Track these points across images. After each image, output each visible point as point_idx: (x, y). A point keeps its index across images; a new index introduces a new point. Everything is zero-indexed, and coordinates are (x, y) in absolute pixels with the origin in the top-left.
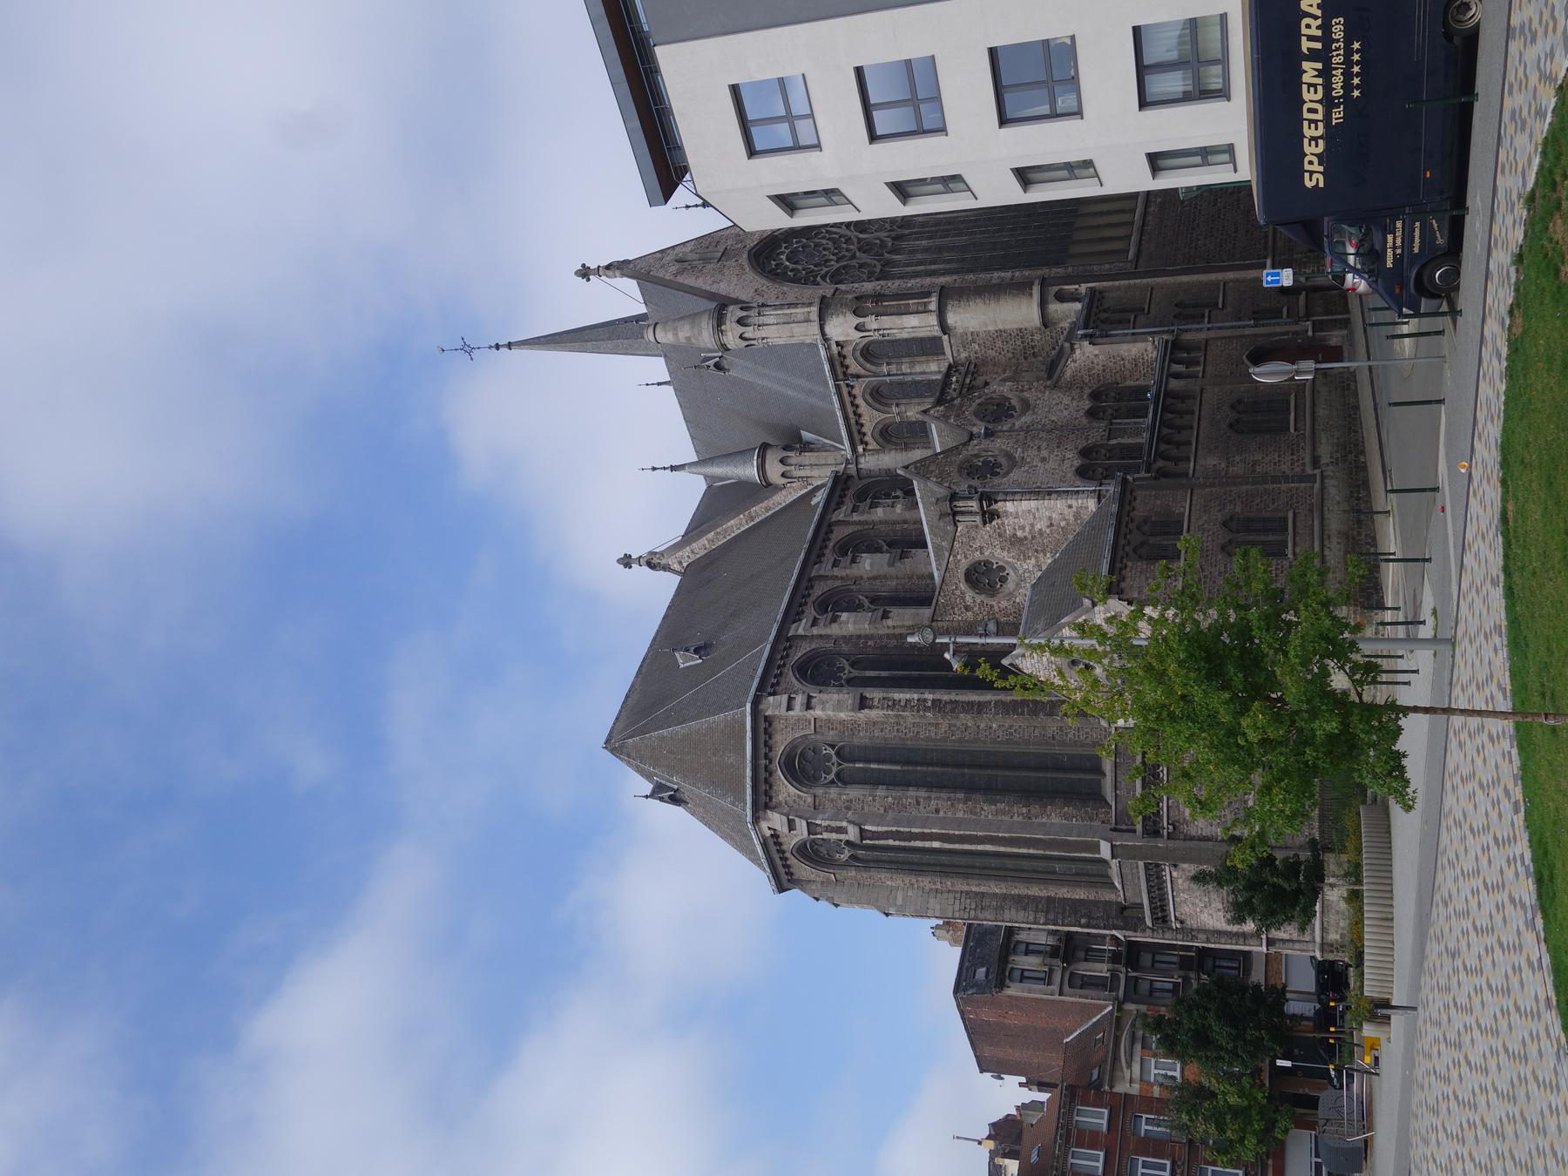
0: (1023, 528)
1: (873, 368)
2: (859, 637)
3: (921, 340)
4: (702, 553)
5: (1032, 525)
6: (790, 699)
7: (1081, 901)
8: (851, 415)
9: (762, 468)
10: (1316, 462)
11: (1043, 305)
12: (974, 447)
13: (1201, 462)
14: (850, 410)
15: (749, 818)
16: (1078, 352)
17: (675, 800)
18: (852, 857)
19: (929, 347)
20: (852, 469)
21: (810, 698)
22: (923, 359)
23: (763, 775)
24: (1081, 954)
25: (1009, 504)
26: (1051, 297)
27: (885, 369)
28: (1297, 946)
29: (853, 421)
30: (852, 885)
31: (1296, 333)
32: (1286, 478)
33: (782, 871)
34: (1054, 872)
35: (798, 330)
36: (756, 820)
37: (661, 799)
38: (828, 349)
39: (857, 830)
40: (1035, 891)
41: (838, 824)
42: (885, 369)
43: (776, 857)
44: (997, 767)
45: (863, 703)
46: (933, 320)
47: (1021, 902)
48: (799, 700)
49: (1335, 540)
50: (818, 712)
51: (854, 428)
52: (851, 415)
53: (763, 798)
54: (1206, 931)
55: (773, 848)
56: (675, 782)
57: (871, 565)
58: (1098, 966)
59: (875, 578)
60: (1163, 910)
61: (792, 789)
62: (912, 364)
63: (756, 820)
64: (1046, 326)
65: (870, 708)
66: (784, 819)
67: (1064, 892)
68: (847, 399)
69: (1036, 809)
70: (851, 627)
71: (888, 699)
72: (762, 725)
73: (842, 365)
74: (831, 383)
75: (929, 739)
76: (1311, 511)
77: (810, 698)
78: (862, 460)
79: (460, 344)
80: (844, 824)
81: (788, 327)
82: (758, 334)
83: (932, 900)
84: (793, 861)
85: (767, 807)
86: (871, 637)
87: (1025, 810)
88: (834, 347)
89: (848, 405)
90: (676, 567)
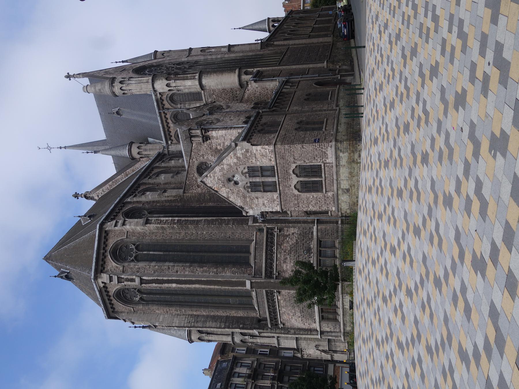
0: (220, 144)
1: (174, 105)
2: (154, 202)
3: (191, 94)
4: (107, 191)
5: (224, 143)
6: (117, 222)
7: (241, 317)
8: (166, 127)
9: (130, 151)
10: (337, 106)
11: (239, 76)
12: (204, 118)
13: (291, 108)
14: (165, 124)
15: (92, 277)
16: (250, 86)
17: (68, 277)
18: (141, 299)
19: (195, 96)
20: (166, 152)
21: (125, 221)
22: (194, 102)
23: (101, 257)
24: (260, 377)
25: (214, 132)
26: (243, 73)
27: (179, 106)
28: (333, 334)
29: (166, 130)
30: (141, 313)
31: (334, 78)
32: (325, 110)
33: (109, 306)
34: (230, 304)
35: (143, 86)
36: (96, 278)
37: (62, 277)
38: (156, 95)
39: (139, 279)
40: (221, 313)
41: (131, 277)
42: (179, 106)
43: (106, 298)
44: (205, 252)
45: (147, 222)
46: (197, 82)
47: (214, 318)
48: (120, 222)
49: (343, 125)
50: (128, 227)
51: (167, 133)
52: (166, 127)
53: (100, 268)
54: (294, 329)
55: (105, 294)
56: (68, 268)
57: (164, 178)
58: (266, 381)
59: (166, 184)
60: (276, 319)
61: (114, 264)
62: (190, 105)
63: (96, 278)
64: (242, 88)
65: (150, 224)
66: (108, 276)
67: (233, 313)
68: (164, 119)
69: (220, 269)
70: (150, 197)
71: (158, 220)
72: (104, 235)
73: (162, 103)
74: (157, 111)
75: (176, 239)
76: (334, 118)
77: (125, 221)
78: (170, 147)
79: (46, 146)
80: (134, 277)
81: (140, 86)
82: (128, 88)
83: (175, 319)
84: (114, 301)
85: (102, 272)
86: (158, 202)
87: (215, 270)
88: (158, 95)
89: (164, 122)
90: (96, 198)
